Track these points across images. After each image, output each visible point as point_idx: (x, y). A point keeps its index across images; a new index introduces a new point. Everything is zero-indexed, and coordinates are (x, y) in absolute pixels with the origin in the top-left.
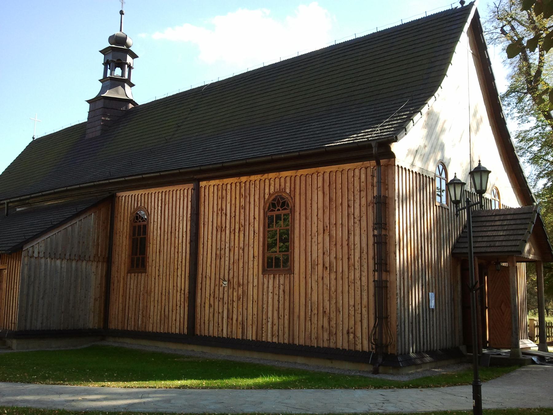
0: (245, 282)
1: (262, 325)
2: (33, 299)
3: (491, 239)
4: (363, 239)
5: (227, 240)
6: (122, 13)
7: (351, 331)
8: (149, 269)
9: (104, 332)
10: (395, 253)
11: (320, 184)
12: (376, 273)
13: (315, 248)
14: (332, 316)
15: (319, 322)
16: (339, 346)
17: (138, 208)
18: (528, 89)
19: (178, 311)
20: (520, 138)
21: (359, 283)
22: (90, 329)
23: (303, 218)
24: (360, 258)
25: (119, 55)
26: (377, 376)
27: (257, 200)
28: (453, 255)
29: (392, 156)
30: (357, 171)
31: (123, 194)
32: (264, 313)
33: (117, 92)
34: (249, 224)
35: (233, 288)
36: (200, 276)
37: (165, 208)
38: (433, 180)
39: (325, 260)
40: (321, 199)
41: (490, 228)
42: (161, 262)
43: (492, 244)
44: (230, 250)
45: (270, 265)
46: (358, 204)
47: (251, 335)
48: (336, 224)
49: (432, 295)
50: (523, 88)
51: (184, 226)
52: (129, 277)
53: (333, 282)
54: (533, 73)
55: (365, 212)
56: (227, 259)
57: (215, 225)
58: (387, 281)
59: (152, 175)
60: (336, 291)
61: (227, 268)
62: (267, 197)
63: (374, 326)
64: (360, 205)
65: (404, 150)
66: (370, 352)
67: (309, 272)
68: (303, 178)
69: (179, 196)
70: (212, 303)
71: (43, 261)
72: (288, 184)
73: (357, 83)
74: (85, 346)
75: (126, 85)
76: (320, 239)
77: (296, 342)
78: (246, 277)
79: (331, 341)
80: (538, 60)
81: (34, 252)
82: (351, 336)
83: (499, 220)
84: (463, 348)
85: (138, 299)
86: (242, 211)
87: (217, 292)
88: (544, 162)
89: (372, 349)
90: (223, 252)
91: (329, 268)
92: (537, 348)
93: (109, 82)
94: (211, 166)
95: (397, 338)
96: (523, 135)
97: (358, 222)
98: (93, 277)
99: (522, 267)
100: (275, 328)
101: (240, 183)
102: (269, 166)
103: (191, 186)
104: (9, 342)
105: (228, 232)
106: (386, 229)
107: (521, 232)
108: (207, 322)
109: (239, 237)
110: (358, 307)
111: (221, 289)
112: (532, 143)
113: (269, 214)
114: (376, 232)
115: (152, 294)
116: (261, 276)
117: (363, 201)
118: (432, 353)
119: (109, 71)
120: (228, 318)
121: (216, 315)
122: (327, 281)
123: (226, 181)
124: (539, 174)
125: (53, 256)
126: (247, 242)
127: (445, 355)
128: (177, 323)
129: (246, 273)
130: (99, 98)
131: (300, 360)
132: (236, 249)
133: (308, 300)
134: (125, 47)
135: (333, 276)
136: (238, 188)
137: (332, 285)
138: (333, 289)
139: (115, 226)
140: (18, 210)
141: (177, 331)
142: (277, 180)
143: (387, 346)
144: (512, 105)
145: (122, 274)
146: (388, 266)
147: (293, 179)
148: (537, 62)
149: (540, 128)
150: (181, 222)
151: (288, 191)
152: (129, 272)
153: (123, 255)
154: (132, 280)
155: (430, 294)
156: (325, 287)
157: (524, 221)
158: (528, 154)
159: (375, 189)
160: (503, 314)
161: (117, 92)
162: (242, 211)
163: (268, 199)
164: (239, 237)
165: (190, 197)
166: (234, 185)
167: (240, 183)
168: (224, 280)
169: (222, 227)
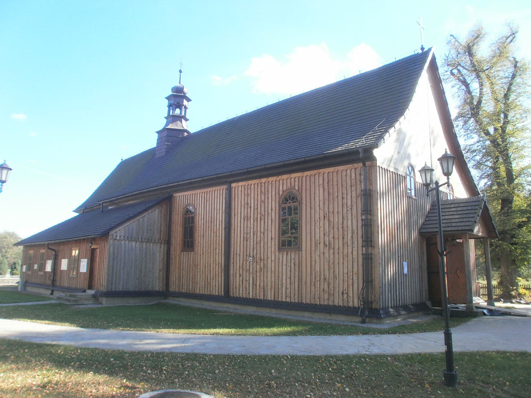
0: (266, 257)
1: (278, 289)
2: (117, 269)
3: (449, 221)
4: (354, 223)
5: (252, 226)
6: (181, 72)
7: (345, 292)
8: (196, 249)
10: (378, 233)
11: (321, 182)
12: (364, 248)
13: (317, 231)
14: (330, 282)
15: (321, 286)
16: (336, 303)
17: (189, 205)
18: (472, 114)
19: (217, 279)
20: (466, 150)
21: (351, 256)
22: (156, 291)
23: (308, 208)
24: (352, 237)
25: (178, 100)
27: (273, 196)
28: (421, 234)
29: (373, 159)
30: (348, 171)
31: (176, 195)
32: (280, 280)
33: (177, 125)
34: (268, 214)
35: (257, 262)
36: (232, 253)
37: (206, 204)
38: (405, 178)
39: (325, 240)
41: (448, 213)
42: (205, 243)
43: (450, 225)
44: (254, 234)
45: (283, 245)
46: (350, 196)
47: (270, 297)
48: (333, 212)
49: (405, 264)
50: (468, 114)
51: (221, 217)
52: (182, 255)
53: (332, 256)
54: (475, 103)
55: (355, 202)
56: (252, 240)
57: (243, 216)
58: (372, 254)
59: (197, 180)
60: (334, 263)
61: (252, 247)
62: (281, 193)
63: (362, 288)
64: (351, 197)
65: (384, 154)
66: (359, 307)
67: (313, 249)
68: (308, 178)
70: (241, 273)
71: (123, 242)
72: (297, 183)
73: (347, 109)
74: (153, 303)
75: (183, 120)
76: (322, 224)
77: (304, 301)
78: (266, 254)
79: (330, 299)
80: (479, 93)
81: (117, 236)
82: (345, 296)
83: (454, 207)
85: (189, 270)
86: (263, 204)
87: (245, 265)
88: (485, 167)
89: (361, 305)
90: (248, 235)
91: (328, 246)
92: (486, 304)
93: (172, 118)
94: (239, 171)
95: (380, 296)
96: (468, 148)
97: (350, 210)
98: (158, 254)
99: (472, 242)
100: (288, 291)
101: (261, 183)
102: (282, 170)
103: (225, 187)
105: (252, 220)
106: (371, 215)
107: (472, 215)
108: (238, 287)
109: (260, 224)
110: (350, 274)
111: (248, 263)
112: (475, 154)
113: (283, 206)
114: (364, 217)
115: (199, 267)
116: (277, 253)
117: (354, 194)
119: (171, 111)
120: (253, 284)
121: (244, 282)
122: (327, 255)
123: (250, 182)
124: (481, 176)
125: (130, 239)
126: (266, 228)
129: (266, 251)
130: (164, 129)
132: (259, 233)
133: (312, 270)
134: (182, 94)
135: (331, 251)
136: (259, 187)
137: (330, 259)
138: (331, 261)
139: (172, 219)
140: (109, 208)
141: (217, 294)
142: (289, 180)
143: (372, 303)
144: (460, 127)
145: (178, 253)
146: (373, 243)
147: (300, 178)
148: (478, 95)
149: (481, 142)
150: (218, 214)
151: (297, 188)
152: (183, 251)
153: (178, 239)
154: (185, 256)
155: (404, 263)
156: (325, 260)
157: (473, 207)
158: (473, 162)
159: (362, 184)
160: (459, 277)
161: (177, 125)
162: (263, 204)
163: (282, 195)
164: (260, 224)
165: (224, 195)
166: (256, 185)
167: (261, 183)
168: (250, 256)
169: (248, 217)
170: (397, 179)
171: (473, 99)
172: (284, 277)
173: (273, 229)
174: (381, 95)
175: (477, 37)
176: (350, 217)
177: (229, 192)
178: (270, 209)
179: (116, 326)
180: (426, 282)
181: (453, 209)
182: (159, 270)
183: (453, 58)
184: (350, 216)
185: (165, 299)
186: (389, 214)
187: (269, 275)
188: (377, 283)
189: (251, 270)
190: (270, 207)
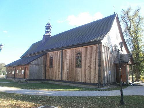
4: (96, 61)
8: (54, 67)
9: (45, 80)
23: (84, 56)
26: (99, 88)
28: (114, 63)
29: (101, 43)
37: (56, 56)
40: (88, 53)
51: (60, 59)
65: (104, 42)
67: (85, 67)
69: (59, 53)
84: (116, 82)
91: (89, 67)
93: (47, 32)
98: (43, 69)
99: (128, 66)
102: (76, 46)
104: (27, 81)
117: (96, 53)
118: (110, 83)
122: (89, 69)
127: (114, 84)
128: (59, 78)
130: (45, 35)
131: (83, 85)
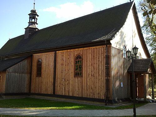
4: (102, 67)
5: (64, 68)
6: (34, 4)
13: (89, 70)
17: (39, 59)
23: (86, 62)
24: (102, 73)
25: (34, 15)
37: (47, 59)
43: (139, 69)
45: (76, 75)
47: (71, 94)
51: (52, 64)
53: (94, 79)
56: (64, 73)
60: (95, 82)
65: (114, 42)
67: (87, 77)
68: (86, 50)
72: (81, 52)
77: (84, 96)
88: (154, 46)
91: (93, 76)
92: (151, 98)
93: (31, 23)
99: (147, 75)
103: (54, 52)
116: (74, 78)
119: (31, 20)
121: (61, 89)
130: (28, 28)
135: (94, 78)
138: (94, 82)
148: (151, 18)
154: (37, 79)
170: (119, 51)
171: (149, 19)
172: (76, 87)
173: (72, 69)
174: (113, 18)
175: (125, 47)
176: (101, 65)
177: (56, 54)
178: (71, 61)
179: (12, 107)
180: (130, 90)
181: (140, 63)
182: (27, 84)
183: (142, 3)
184: (101, 65)
185: (29, 96)
186: (116, 63)
187: (71, 86)
188: (111, 89)
189: (64, 84)
190: (71, 60)
